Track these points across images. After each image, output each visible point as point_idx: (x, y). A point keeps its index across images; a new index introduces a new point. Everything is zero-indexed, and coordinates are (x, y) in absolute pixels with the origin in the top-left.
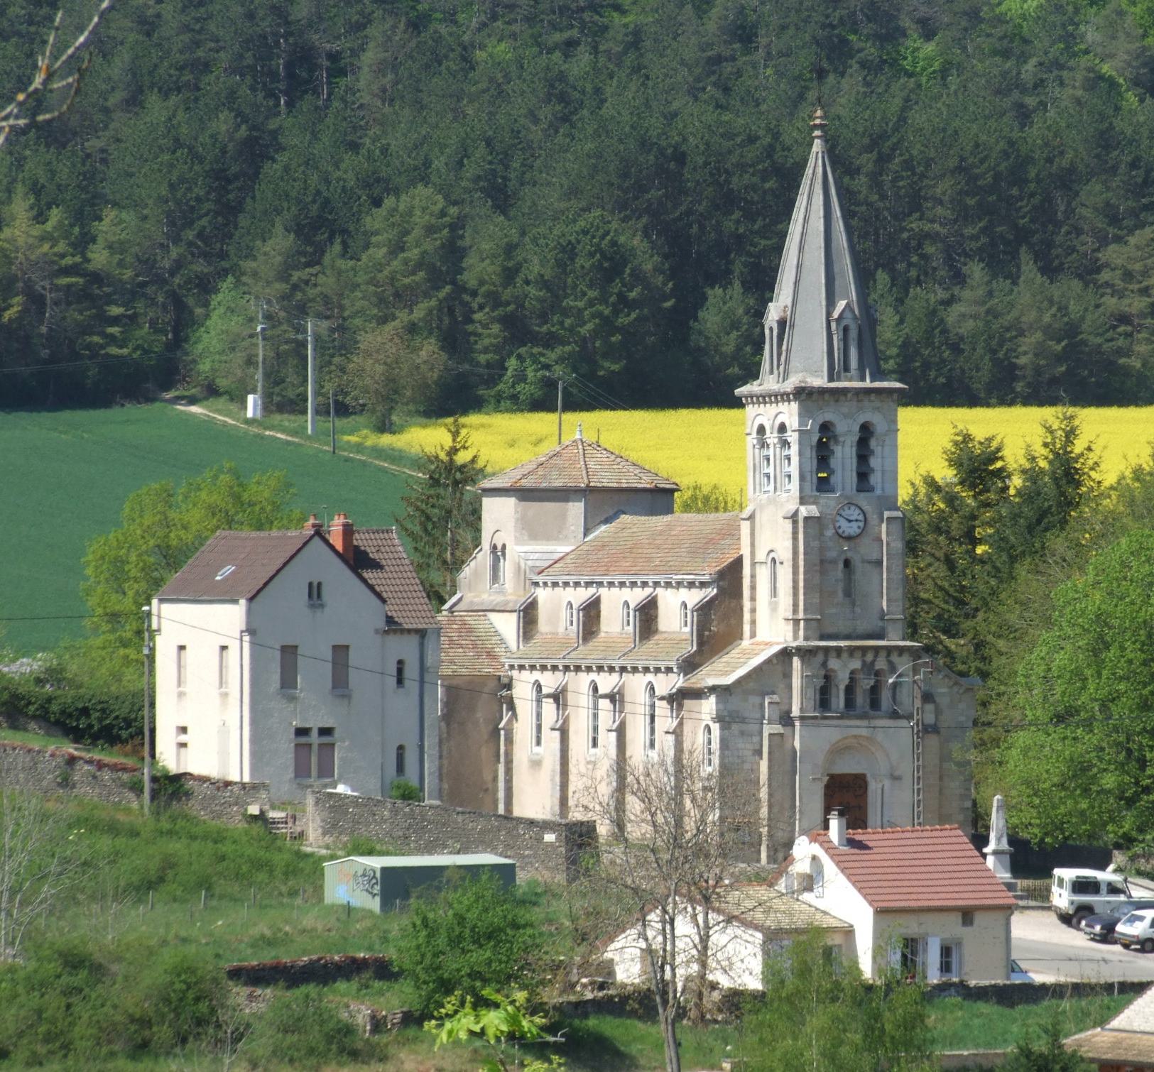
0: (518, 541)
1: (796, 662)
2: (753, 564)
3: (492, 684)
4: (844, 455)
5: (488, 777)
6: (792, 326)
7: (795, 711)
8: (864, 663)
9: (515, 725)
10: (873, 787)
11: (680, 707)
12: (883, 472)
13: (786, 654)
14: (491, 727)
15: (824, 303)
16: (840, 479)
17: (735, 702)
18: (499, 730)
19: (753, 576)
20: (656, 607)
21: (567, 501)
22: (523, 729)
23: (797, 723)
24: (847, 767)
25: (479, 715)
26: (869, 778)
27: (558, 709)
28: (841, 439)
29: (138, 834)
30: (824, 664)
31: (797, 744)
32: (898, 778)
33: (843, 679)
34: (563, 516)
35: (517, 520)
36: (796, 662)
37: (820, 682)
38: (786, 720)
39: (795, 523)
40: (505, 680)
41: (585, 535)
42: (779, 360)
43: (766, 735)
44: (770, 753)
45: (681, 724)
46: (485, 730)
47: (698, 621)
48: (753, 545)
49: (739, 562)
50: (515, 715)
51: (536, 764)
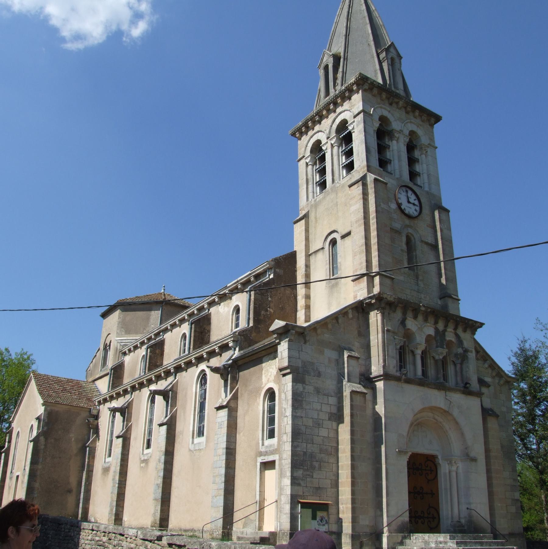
0: (118, 335)
1: (375, 318)
2: (308, 256)
3: (84, 414)
4: (397, 149)
5: (73, 481)
6: (346, 59)
7: (376, 369)
8: (437, 330)
9: (97, 444)
10: (444, 468)
11: (235, 380)
12: (429, 175)
13: (361, 309)
14: (80, 445)
15: (372, 43)
16: (397, 167)
17: (309, 353)
18: (86, 447)
19: (307, 266)
20: (209, 324)
21: (150, 310)
22: (101, 446)
23: (380, 385)
24: (425, 446)
25: (72, 435)
26: (440, 460)
27: (124, 421)
28: (397, 135)
29: (259, 530)
30: (403, 323)
31: (380, 408)
32: (474, 460)
33: (420, 340)
34: (148, 319)
35: (119, 323)
36: (375, 318)
37: (399, 340)
38: (368, 380)
39: (365, 185)
40: (94, 412)
41: (161, 324)
42: (335, 79)
43: (347, 394)
44: (352, 415)
45: (235, 397)
46: (74, 447)
47: (255, 299)
48: (307, 239)
49: (292, 256)
50: (98, 436)
51: (106, 470)
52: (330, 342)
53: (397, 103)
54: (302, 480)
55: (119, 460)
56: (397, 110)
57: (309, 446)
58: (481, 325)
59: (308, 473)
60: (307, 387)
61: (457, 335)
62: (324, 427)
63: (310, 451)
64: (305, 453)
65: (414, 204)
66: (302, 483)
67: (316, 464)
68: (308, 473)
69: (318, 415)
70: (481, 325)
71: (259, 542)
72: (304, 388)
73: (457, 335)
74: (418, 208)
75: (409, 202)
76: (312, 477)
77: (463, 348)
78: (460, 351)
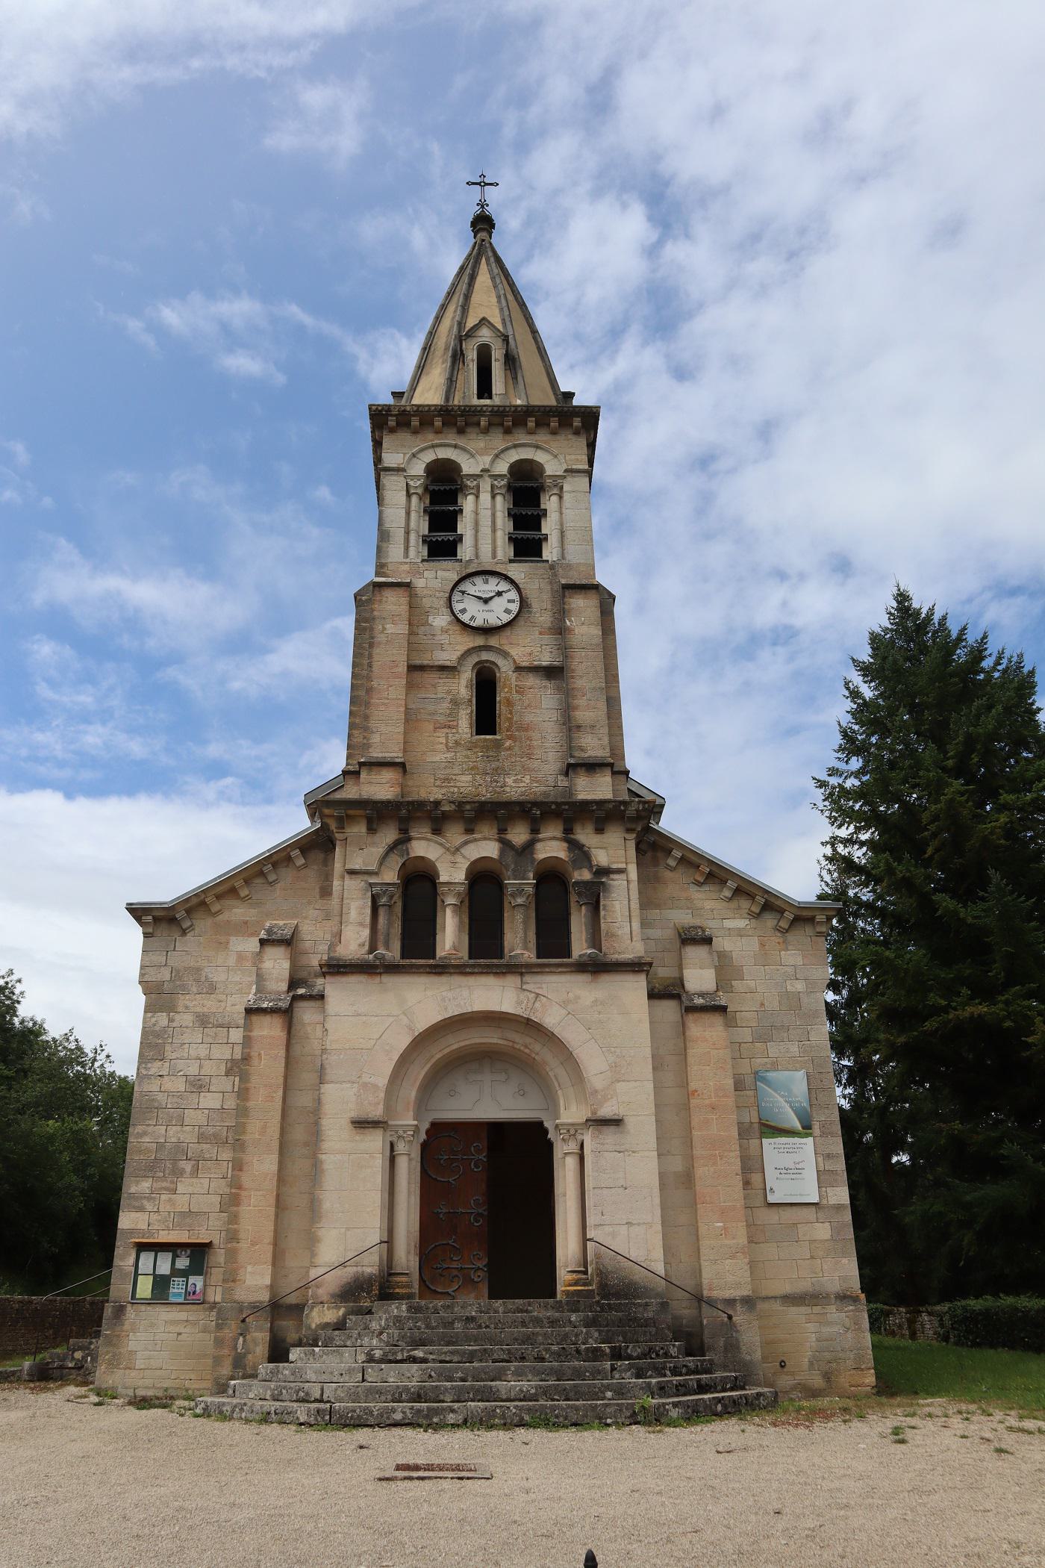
52: (246, 923)
53: (478, 424)
54: (149, 1199)
55: (590, 1438)
56: (481, 436)
57: (172, 1130)
58: (902, 598)
59: (164, 1184)
60: (177, 1017)
61: (574, 846)
62: (212, 1089)
63: (174, 1140)
64: (160, 1146)
65: (499, 594)
66: (149, 1206)
67: (188, 1167)
68: (164, 1184)
69: (201, 1067)
70: (902, 598)
71: (654, 236)
72: (171, 1020)
73: (574, 846)
74: (513, 595)
75: (486, 601)
76: (174, 1191)
77: (591, 867)
78: (586, 875)
